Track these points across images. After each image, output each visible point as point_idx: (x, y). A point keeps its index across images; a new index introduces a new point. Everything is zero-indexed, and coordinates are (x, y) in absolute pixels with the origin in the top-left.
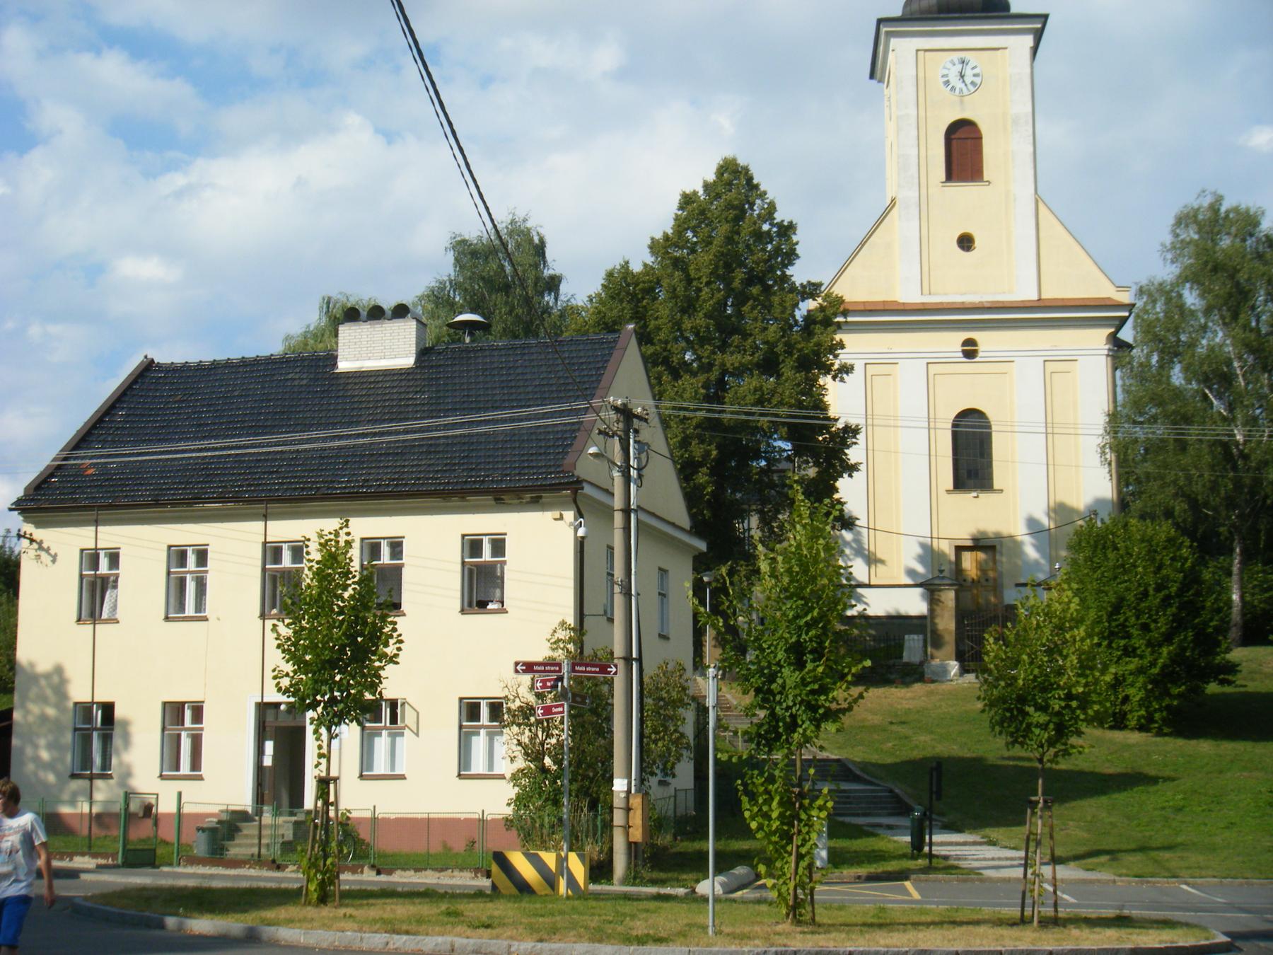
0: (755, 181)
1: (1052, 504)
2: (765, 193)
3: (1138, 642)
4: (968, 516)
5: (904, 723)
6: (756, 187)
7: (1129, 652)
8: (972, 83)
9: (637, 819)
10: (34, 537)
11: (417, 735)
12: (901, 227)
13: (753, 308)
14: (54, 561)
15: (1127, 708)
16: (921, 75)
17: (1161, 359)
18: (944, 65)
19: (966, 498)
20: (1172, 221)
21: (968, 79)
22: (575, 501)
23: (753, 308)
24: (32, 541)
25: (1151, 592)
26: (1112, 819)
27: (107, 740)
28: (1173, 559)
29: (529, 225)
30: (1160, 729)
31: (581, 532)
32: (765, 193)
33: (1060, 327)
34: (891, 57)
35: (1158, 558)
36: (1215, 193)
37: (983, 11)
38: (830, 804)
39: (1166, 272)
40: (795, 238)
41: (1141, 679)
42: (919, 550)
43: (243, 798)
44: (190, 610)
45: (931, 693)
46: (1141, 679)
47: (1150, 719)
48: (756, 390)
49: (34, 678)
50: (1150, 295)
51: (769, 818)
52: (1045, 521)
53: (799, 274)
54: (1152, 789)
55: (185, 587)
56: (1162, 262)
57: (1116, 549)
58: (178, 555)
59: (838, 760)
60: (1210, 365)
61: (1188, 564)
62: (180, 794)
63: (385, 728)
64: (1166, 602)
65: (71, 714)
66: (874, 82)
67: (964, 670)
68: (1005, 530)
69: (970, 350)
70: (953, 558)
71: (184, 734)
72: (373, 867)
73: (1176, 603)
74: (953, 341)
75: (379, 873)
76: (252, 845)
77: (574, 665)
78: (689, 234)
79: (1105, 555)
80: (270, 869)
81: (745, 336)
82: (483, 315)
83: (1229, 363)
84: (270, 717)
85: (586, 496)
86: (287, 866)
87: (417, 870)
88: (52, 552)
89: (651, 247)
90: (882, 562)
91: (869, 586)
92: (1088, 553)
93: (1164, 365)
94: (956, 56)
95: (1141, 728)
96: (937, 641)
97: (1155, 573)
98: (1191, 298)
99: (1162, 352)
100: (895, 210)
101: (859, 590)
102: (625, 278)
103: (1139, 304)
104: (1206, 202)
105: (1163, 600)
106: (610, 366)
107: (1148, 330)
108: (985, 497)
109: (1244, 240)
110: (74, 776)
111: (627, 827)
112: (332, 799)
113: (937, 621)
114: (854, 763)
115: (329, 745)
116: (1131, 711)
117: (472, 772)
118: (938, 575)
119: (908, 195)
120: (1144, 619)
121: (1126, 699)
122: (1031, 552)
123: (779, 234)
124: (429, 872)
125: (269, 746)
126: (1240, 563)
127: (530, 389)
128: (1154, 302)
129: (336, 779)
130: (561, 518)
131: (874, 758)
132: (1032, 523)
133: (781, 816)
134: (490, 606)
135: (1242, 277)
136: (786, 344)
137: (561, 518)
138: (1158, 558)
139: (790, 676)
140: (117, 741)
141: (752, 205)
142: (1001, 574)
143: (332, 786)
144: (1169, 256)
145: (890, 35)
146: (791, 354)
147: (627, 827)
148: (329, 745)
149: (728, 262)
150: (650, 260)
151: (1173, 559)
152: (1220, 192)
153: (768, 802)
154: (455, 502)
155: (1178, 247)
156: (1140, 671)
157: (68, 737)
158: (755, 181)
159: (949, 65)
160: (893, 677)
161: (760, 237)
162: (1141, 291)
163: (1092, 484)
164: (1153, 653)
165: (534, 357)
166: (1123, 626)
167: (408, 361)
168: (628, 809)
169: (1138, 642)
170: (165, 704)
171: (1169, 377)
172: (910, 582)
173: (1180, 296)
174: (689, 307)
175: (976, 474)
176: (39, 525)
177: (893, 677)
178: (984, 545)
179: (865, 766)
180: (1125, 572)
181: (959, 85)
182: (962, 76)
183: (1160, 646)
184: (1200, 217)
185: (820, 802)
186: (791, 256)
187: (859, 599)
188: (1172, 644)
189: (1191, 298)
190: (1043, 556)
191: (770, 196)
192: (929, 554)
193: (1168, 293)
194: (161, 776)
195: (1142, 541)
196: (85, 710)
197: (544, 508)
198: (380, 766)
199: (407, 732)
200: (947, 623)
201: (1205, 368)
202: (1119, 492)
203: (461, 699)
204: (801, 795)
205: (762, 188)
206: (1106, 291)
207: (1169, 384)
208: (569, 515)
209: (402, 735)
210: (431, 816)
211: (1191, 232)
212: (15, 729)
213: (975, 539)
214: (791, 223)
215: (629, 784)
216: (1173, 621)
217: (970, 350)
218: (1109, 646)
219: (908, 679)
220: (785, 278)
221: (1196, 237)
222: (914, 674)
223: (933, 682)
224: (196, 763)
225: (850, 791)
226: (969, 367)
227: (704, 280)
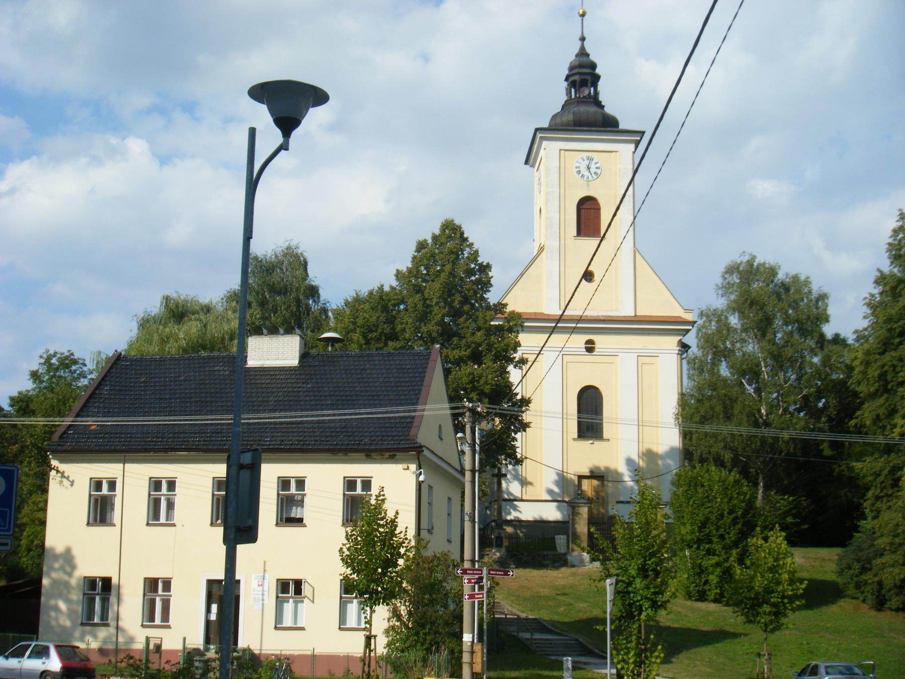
0: (465, 236)
2: (472, 244)
3: (718, 547)
4: (585, 457)
5: (565, 594)
6: (466, 239)
7: (710, 552)
8: (595, 173)
9: (478, 658)
10: (60, 469)
11: (313, 602)
12: (547, 265)
13: (467, 320)
14: (72, 485)
15: (707, 587)
17: (713, 359)
18: (577, 161)
19: (586, 444)
20: (722, 269)
22: (418, 459)
23: (467, 320)
24: (58, 471)
25: (726, 515)
26: (721, 660)
27: (105, 602)
28: (738, 493)
29: (299, 251)
30: (728, 601)
31: (422, 478)
32: (472, 244)
33: (649, 334)
34: (542, 153)
35: (729, 493)
36: (751, 254)
37: (603, 126)
38: (662, 655)
39: (720, 303)
40: (490, 274)
41: (718, 570)
42: (555, 477)
43: (197, 640)
44: (163, 519)
45: (574, 574)
46: (718, 570)
47: (722, 595)
48: (470, 374)
49: (56, 557)
50: (708, 316)
51: (627, 663)
53: (492, 297)
54: (738, 640)
55: (160, 504)
56: (715, 296)
57: (703, 486)
58: (156, 484)
59: (535, 619)
60: (747, 365)
61: (748, 497)
62: (185, 639)
63: (291, 597)
64: (735, 521)
66: (527, 166)
67: (593, 560)
68: (613, 466)
69: (590, 347)
70: (577, 483)
71: (158, 599)
73: (741, 521)
74: (579, 341)
77: (490, 570)
78: (422, 268)
79: (696, 490)
81: (462, 338)
82: (340, 333)
83: (758, 365)
84: (215, 589)
85: (425, 456)
88: (71, 479)
89: (397, 276)
90: (531, 484)
91: (522, 500)
92: (685, 488)
93: (715, 364)
94: (585, 155)
95: (715, 601)
96: (575, 537)
97: (728, 503)
98: (734, 320)
99: (714, 354)
101: (515, 503)
102: (381, 297)
103: (700, 322)
104: (745, 259)
105: (733, 520)
106: (428, 370)
107: (708, 342)
108: (598, 444)
109: (768, 285)
110: (82, 624)
111: (471, 664)
112: (373, 647)
113: (576, 526)
114: (546, 621)
115: (371, 617)
116: (709, 590)
117: (284, 625)
118: (570, 492)
119: (552, 244)
120: (721, 531)
121: (706, 582)
123: (479, 270)
125: (214, 608)
126: (763, 492)
127: (377, 384)
128: (710, 321)
129: (375, 636)
130: (408, 468)
131: (556, 618)
132: (629, 461)
133: (635, 662)
135: (769, 309)
136: (488, 344)
137: (408, 468)
138: (729, 493)
139: (639, 583)
140: (113, 599)
141: (462, 251)
142: (607, 494)
143: (373, 641)
144: (720, 292)
146: (491, 351)
147: (471, 664)
148: (371, 617)
149: (449, 290)
150: (395, 283)
151: (738, 493)
152: (754, 254)
153: (627, 653)
154: (341, 456)
155: (726, 288)
156: (718, 564)
158: (465, 236)
159: (581, 161)
160: (546, 563)
161: (471, 272)
162: (701, 314)
163: (668, 438)
164: (726, 553)
165: (377, 362)
166: (708, 535)
167: (295, 362)
168: (472, 653)
169: (718, 547)
170: (145, 579)
171: (719, 371)
172: (549, 498)
173: (726, 318)
174: (423, 317)
175: (593, 429)
176: (62, 461)
177: (546, 563)
178: (596, 475)
179: (553, 623)
180: (709, 501)
181: (587, 174)
182: (589, 168)
183: (731, 549)
184: (741, 269)
185: (656, 654)
186: (486, 284)
187: (515, 508)
188: (738, 548)
189: (734, 320)
191: (476, 247)
192: (562, 480)
193: (719, 317)
194: (143, 626)
195: (719, 481)
196: (91, 582)
197: (397, 462)
198: (288, 621)
199: (306, 600)
200: (582, 527)
201: (744, 367)
202: (684, 444)
204: (646, 650)
205: (470, 240)
206: (677, 311)
207: (719, 376)
208: (413, 467)
209: (303, 602)
210: (283, 653)
211: (735, 278)
212: (43, 591)
213: (591, 472)
214: (488, 264)
215: (473, 637)
216: (739, 533)
217: (590, 347)
218: (698, 548)
219: (556, 564)
220: (483, 299)
221: (738, 281)
222: (561, 561)
223: (573, 566)
224: (166, 616)
225: (552, 640)
226: (589, 358)
227: (435, 300)
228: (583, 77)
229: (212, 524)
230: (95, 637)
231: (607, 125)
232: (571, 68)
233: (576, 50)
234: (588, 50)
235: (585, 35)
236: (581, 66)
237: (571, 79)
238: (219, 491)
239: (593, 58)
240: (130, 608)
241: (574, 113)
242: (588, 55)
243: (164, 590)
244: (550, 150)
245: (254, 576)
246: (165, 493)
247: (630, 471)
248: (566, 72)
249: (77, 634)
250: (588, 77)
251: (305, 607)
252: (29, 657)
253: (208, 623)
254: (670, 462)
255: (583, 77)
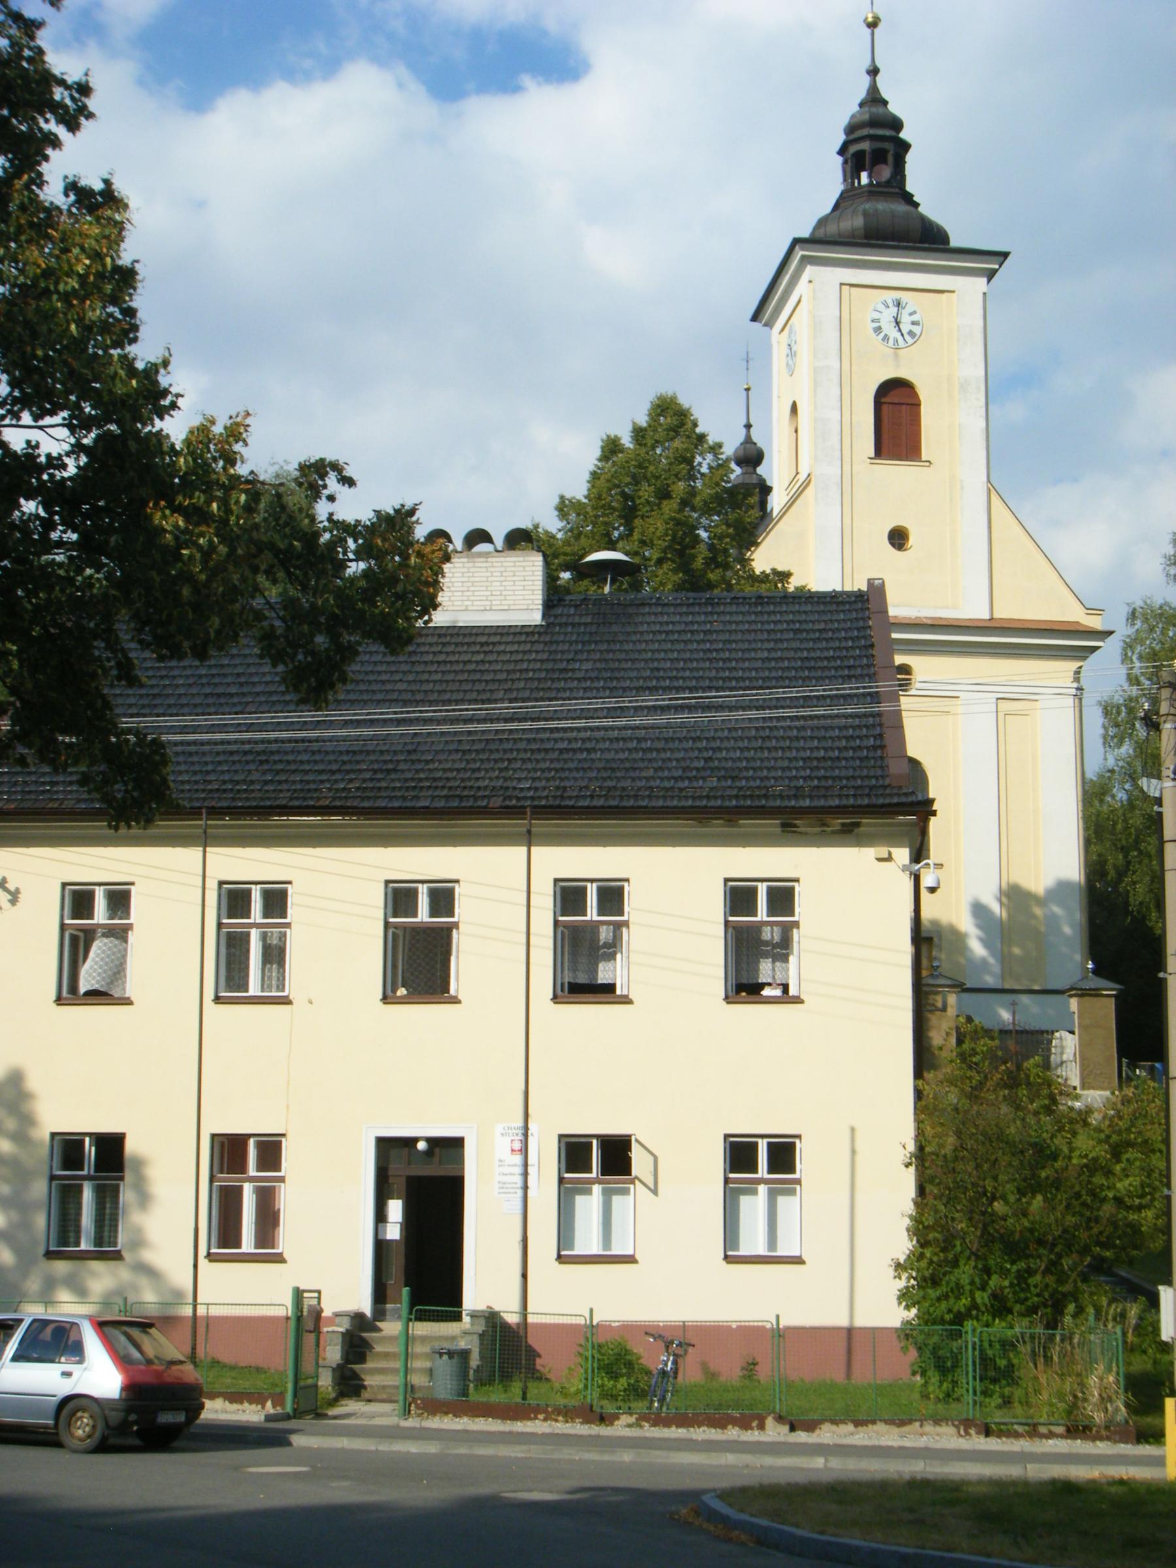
1: (1004, 885)
6: (702, 438)
11: (655, 1192)
16: (845, 316)
18: (871, 307)
21: (905, 328)
27: (108, 1199)
32: (720, 445)
52: (996, 908)
55: (246, 950)
58: (235, 899)
65: (45, 1151)
71: (248, 1190)
72: (780, 1419)
75: (793, 1429)
76: (395, 1371)
80: (587, 1421)
86: (616, 1417)
87: (858, 1423)
88: (11, 886)
100: (810, 491)
110: (50, 1255)
117: (741, 1253)
122: (977, 948)
124: (881, 1427)
125: (395, 1209)
132: (979, 910)
134: (766, 992)
137: (889, 859)
140: (127, 1195)
145: (806, 260)
154: (717, 826)
157: (39, 1189)
159: (881, 307)
170: (454, 1145)
181: (894, 333)
182: (897, 323)
190: (993, 954)
196: (69, 1148)
203: (561, 1136)
205: (711, 440)
206: (1075, 614)
228: (879, 145)
229: (385, 999)
230: (81, 1292)
231: (928, 239)
232: (851, 129)
233: (861, 93)
234: (755, 439)
235: (878, 64)
236: (873, 123)
237: (853, 149)
238: (395, 916)
239: (894, 108)
240: (168, 1215)
241: (865, 214)
242: (885, 103)
243: (261, 1167)
244: (820, 286)
245: (499, 1129)
246: (260, 920)
247: (979, 926)
248: (841, 138)
249: (33, 1285)
250: (889, 146)
251: (631, 1205)
252: (16, 1358)
253: (381, 1247)
254: (1057, 910)
255: (879, 145)
